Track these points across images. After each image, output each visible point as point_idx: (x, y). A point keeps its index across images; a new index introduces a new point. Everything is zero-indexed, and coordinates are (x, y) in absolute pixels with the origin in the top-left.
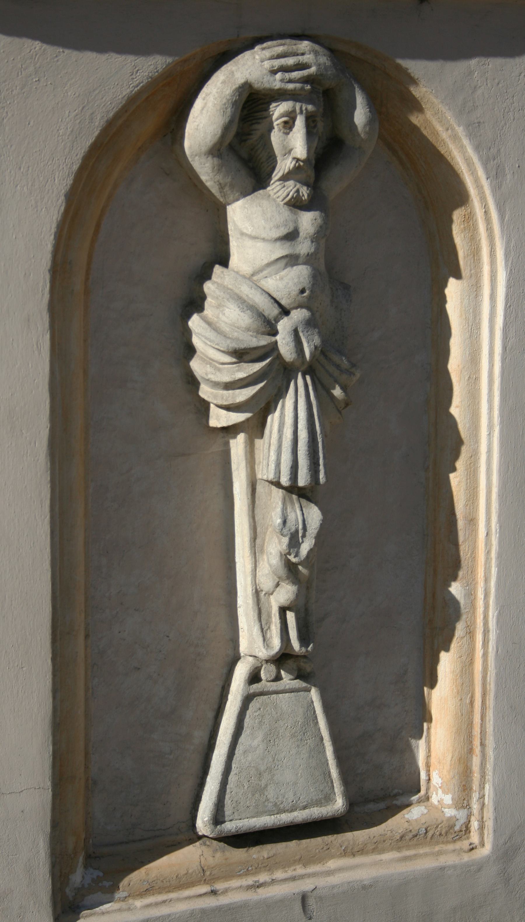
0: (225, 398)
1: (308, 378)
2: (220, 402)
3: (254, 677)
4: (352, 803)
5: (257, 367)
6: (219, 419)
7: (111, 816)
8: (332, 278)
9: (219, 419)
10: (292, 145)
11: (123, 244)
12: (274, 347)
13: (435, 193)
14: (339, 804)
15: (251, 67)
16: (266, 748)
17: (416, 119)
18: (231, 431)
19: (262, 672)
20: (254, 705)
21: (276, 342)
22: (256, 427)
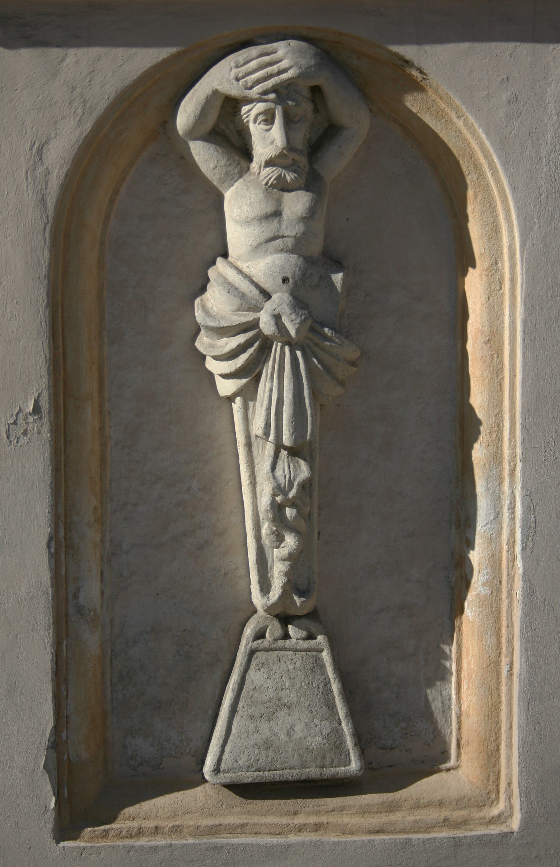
0: (444, 121)
1: (299, 353)
2: (216, 353)
3: (260, 635)
4: (368, 764)
5: (241, 339)
6: (226, 388)
7: (115, 743)
8: (319, 261)
9: (226, 388)
10: (267, 140)
11: (118, 234)
12: (255, 325)
13: (440, 182)
14: (354, 766)
15: (222, 78)
16: (275, 701)
17: (412, 102)
18: (230, 399)
19: (268, 631)
20: (259, 656)
21: (259, 319)
22: (248, 393)
